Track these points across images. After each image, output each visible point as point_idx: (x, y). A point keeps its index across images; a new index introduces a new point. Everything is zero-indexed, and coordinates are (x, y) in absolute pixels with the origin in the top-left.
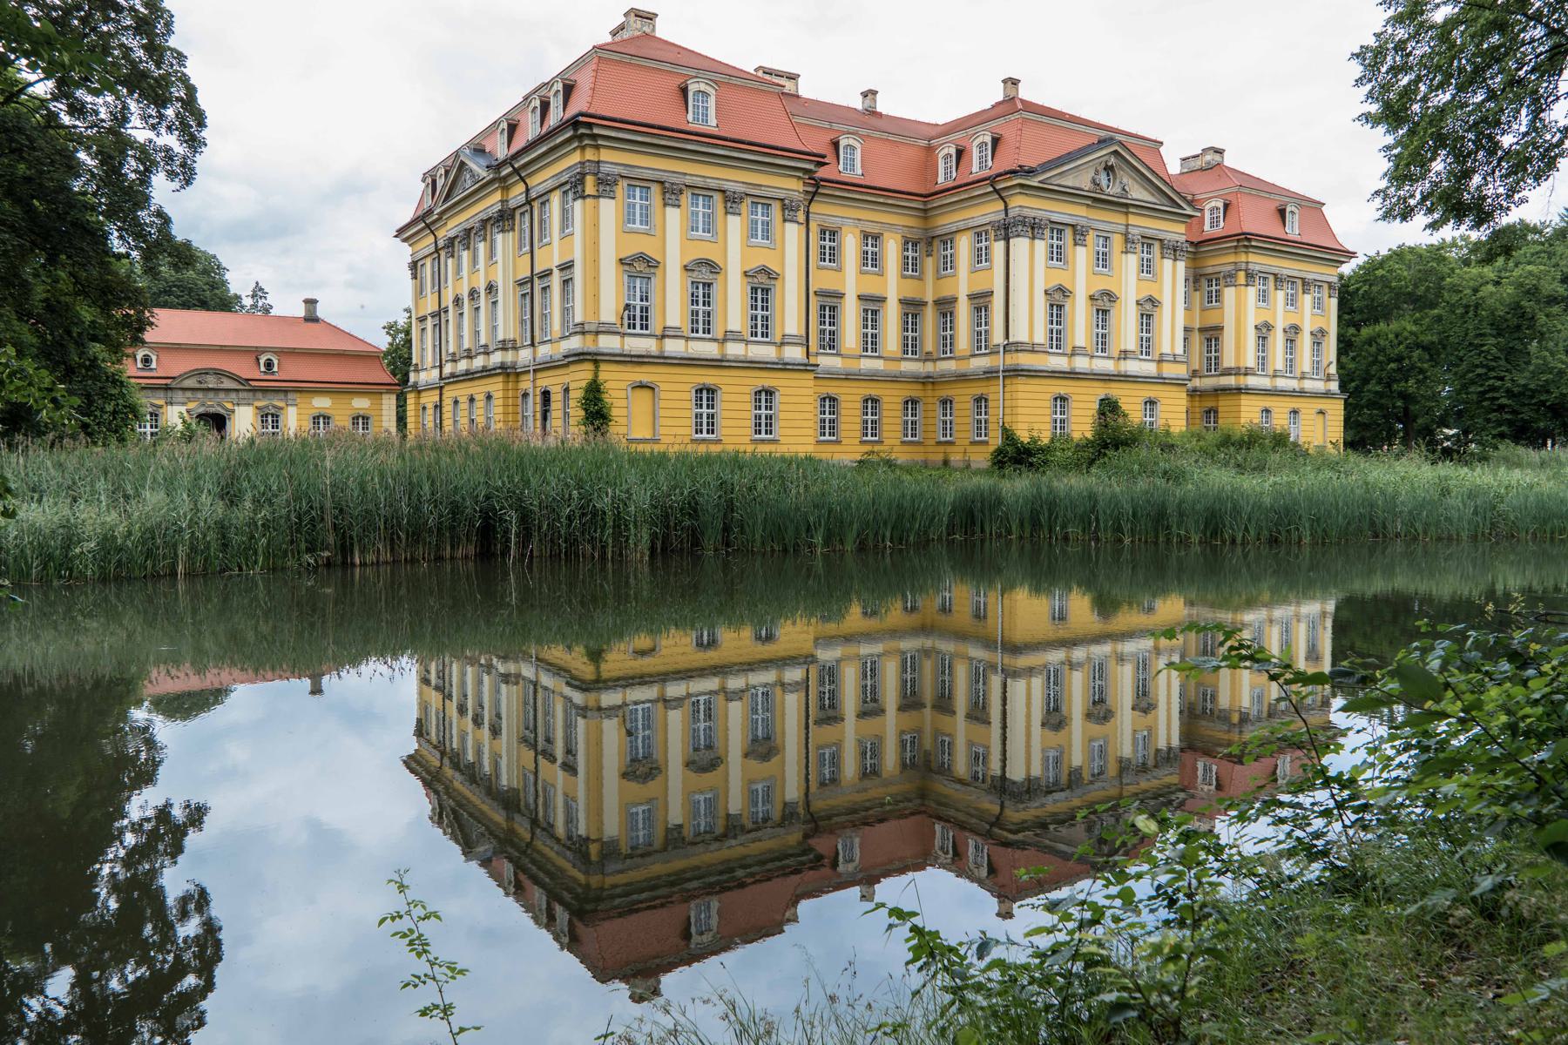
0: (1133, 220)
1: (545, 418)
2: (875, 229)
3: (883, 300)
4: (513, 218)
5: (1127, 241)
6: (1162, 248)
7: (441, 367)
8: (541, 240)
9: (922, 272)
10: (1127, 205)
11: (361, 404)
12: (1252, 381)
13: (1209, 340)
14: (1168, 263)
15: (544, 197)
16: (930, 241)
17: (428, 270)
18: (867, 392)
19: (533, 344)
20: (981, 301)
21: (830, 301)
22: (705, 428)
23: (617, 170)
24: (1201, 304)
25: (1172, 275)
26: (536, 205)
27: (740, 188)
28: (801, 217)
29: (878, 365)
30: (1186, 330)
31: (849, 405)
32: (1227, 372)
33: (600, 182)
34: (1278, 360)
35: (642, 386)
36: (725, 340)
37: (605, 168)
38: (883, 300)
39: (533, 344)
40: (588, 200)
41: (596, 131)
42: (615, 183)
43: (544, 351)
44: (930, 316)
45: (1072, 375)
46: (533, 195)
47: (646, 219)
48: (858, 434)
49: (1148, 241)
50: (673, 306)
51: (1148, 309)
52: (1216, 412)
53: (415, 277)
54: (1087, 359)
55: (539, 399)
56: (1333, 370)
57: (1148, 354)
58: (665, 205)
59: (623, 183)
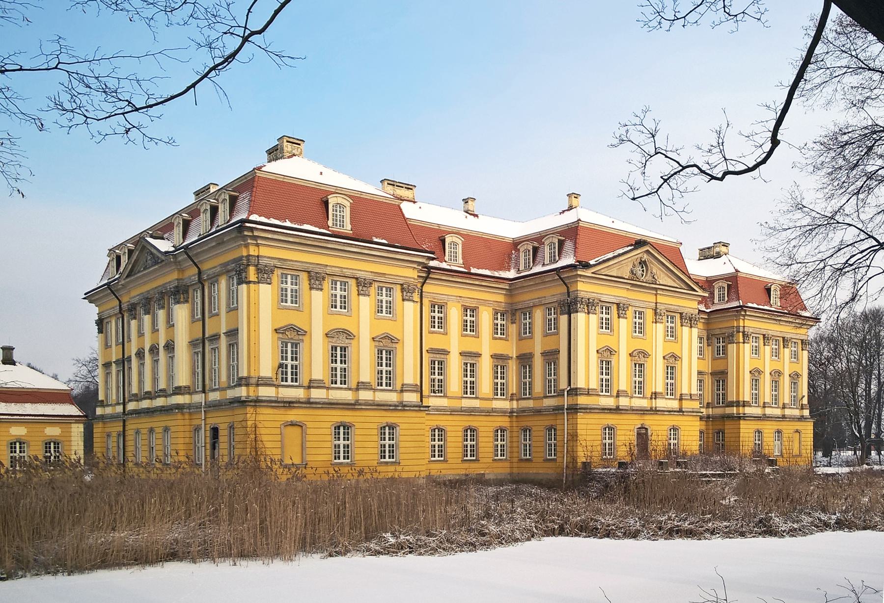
0: (660, 299)
1: (214, 447)
2: (473, 305)
3: (478, 355)
4: (187, 292)
5: (656, 314)
6: (681, 318)
7: (124, 404)
8: (210, 311)
9: (508, 335)
10: (656, 289)
11: (53, 431)
12: (748, 410)
13: (718, 381)
14: (686, 329)
15: (214, 279)
16: (514, 312)
17: (112, 326)
20: (551, 356)
21: (439, 357)
23: (273, 262)
24: (712, 355)
25: (690, 338)
27: (370, 276)
28: (416, 297)
29: (476, 404)
30: (700, 373)
31: (453, 434)
32: (731, 404)
33: (259, 271)
34: (767, 395)
35: (293, 424)
36: (357, 389)
38: (478, 355)
40: (252, 285)
41: (256, 233)
42: (272, 272)
43: (214, 396)
45: (617, 410)
47: (295, 299)
49: (671, 313)
50: (317, 363)
51: (672, 361)
52: (723, 433)
53: (100, 331)
54: (628, 399)
56: (805, 401)
57: (672, 394)
58: (311, 288)
59: (277, 272)
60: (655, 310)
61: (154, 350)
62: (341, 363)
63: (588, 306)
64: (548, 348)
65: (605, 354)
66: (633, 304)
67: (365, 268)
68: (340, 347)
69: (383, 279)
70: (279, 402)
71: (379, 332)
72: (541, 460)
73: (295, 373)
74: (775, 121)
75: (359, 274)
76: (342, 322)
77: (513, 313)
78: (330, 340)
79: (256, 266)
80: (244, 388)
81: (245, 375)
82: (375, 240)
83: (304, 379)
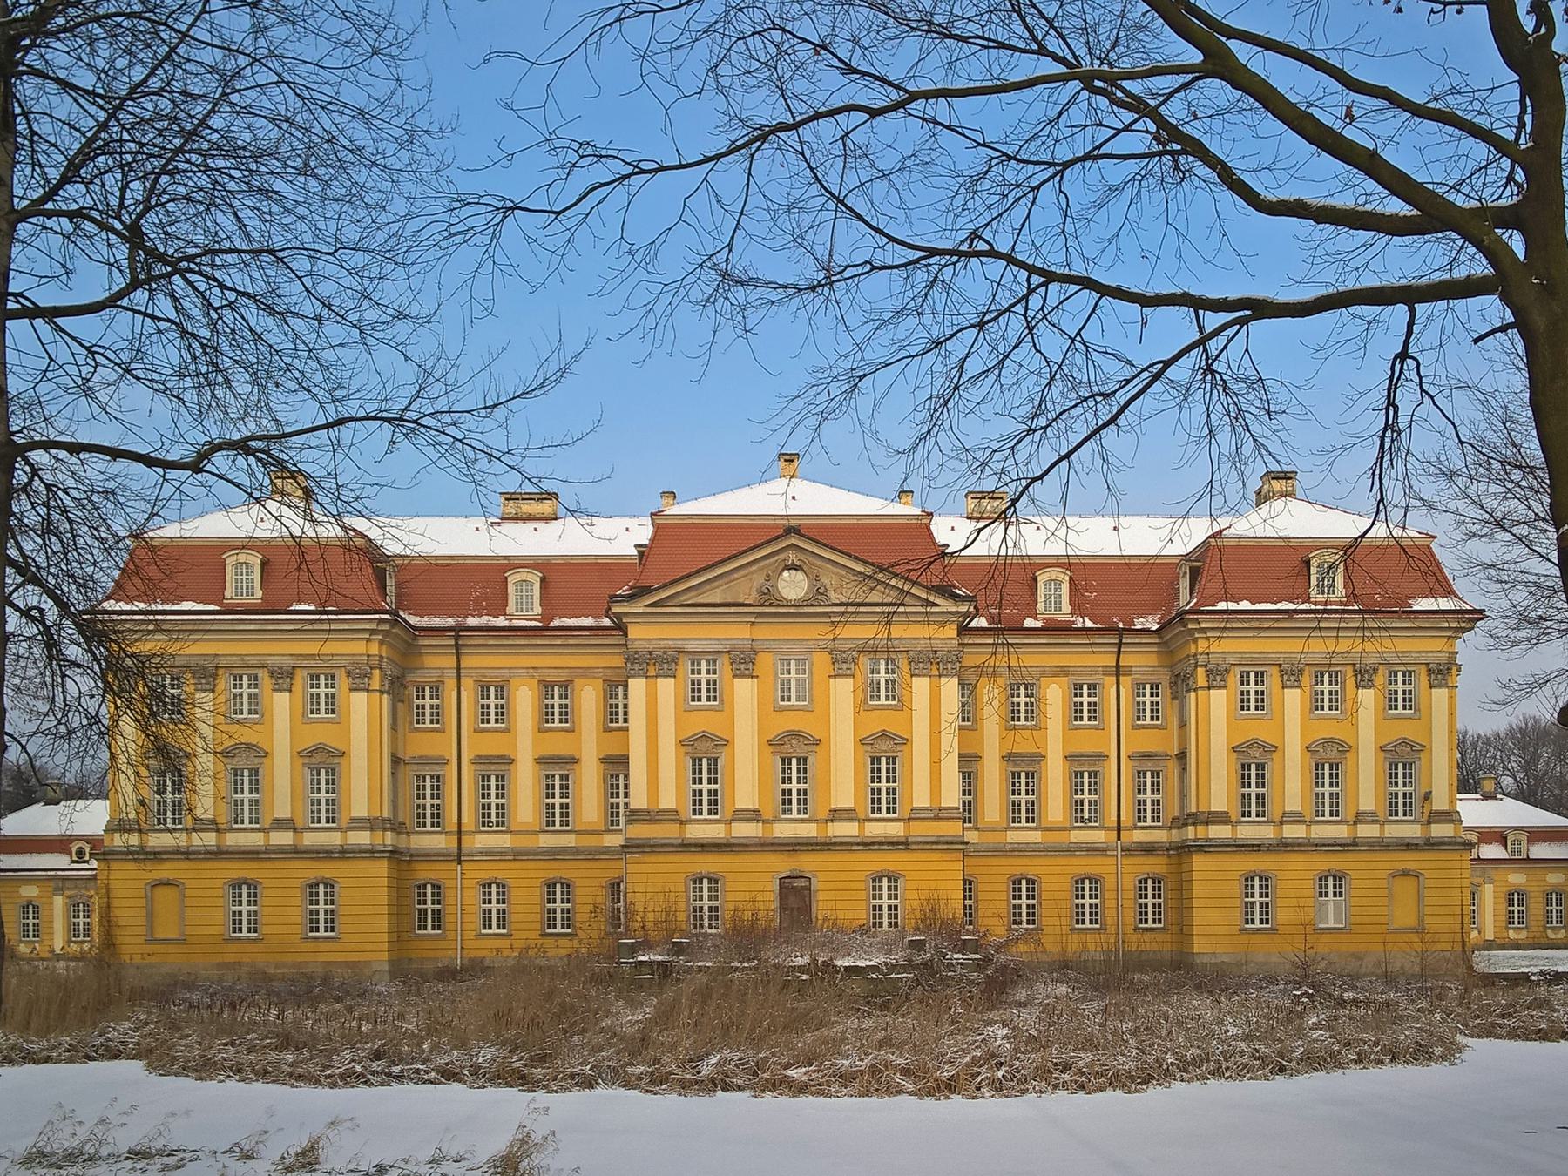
3: (574, 760)
33: (1209, 673)
35: (1406, 874)
38: (574, 760)
44: (1171, 770)
66: (689, 648)
67: (280, 650)
68: (1328, 762)
69: (312, 663)
70: (1456, 844)
71: (1390, 738)
73: (1335, 805)
74: (1179, 291)
75: (270, 661)
76: (1410, 731)
80: (1190, 828)
81: (1194, 810)
82: (295, 607)
83: (1275, 812)
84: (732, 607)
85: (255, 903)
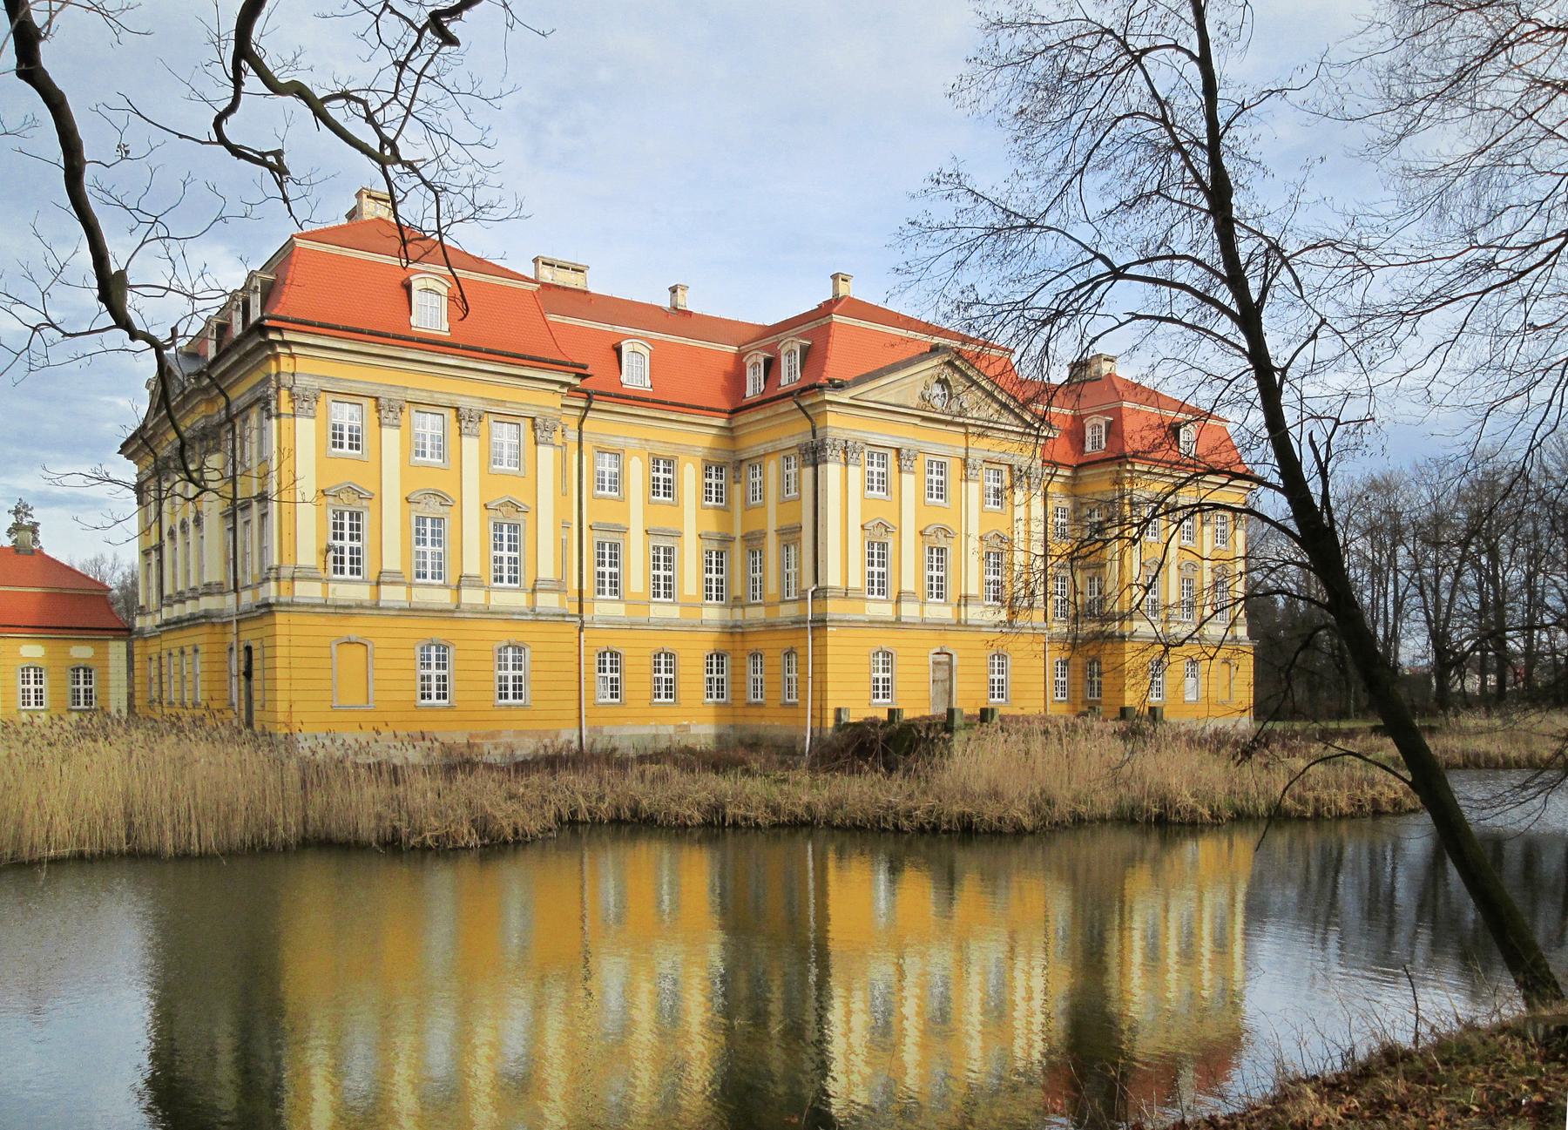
2: (667, 452)
9: (728, 502)
18: (659, 645)
19: (236, 590)
22: (510, 692)
23: (317, 384)
26: (238, 422)
27: (478, 405)
29: (673, 612)
33: (293, 397)
37: (301, 382)
39: (236, 590)
46: (234, 410)
48: (648, 695)
55: (242, 656)
60: (965, 460)
61: (184, 524)
62: (433, 544)
63: (846, 453)
64: (786, 523)
65: (877, 532)
71: (496, 498)
72: (777, 704)
77: (729, 466)
78: (414, 506)
79: (290, 389)
81: (276, 563)
84: (895, 411)
85: (444, 667)
